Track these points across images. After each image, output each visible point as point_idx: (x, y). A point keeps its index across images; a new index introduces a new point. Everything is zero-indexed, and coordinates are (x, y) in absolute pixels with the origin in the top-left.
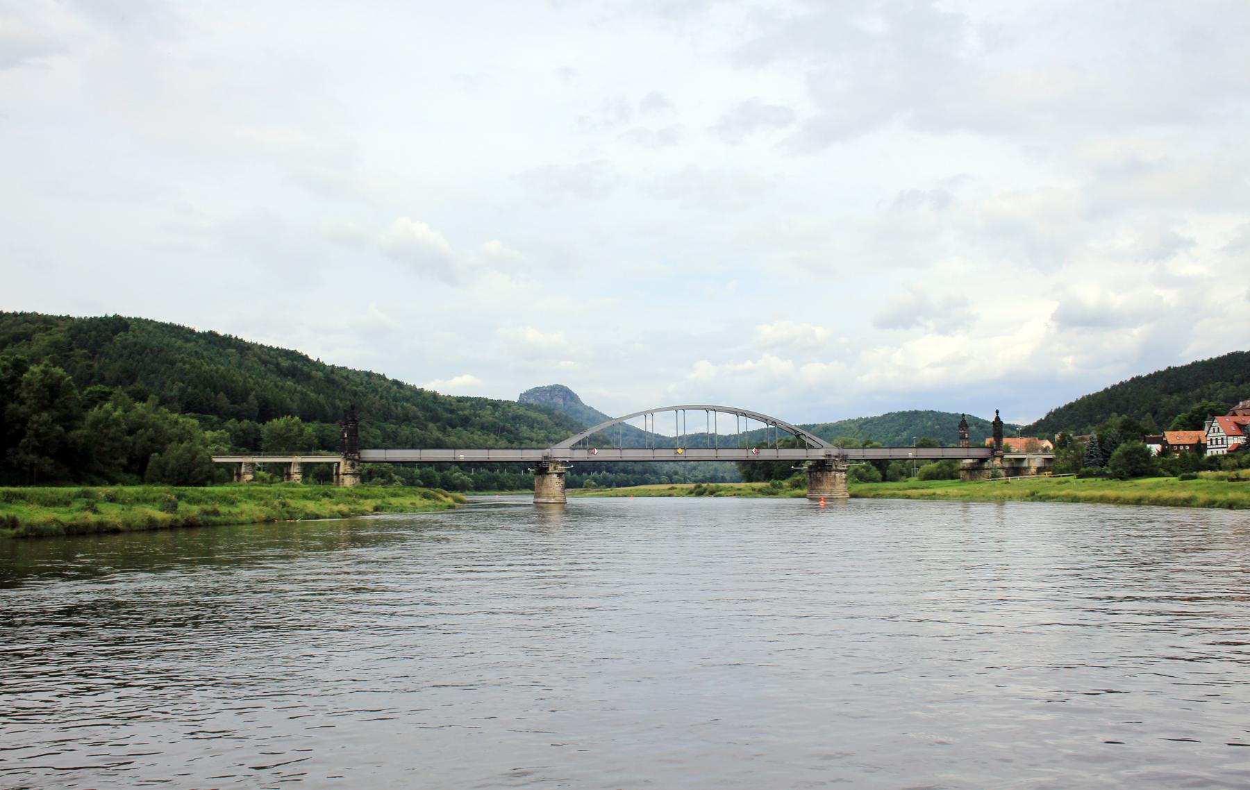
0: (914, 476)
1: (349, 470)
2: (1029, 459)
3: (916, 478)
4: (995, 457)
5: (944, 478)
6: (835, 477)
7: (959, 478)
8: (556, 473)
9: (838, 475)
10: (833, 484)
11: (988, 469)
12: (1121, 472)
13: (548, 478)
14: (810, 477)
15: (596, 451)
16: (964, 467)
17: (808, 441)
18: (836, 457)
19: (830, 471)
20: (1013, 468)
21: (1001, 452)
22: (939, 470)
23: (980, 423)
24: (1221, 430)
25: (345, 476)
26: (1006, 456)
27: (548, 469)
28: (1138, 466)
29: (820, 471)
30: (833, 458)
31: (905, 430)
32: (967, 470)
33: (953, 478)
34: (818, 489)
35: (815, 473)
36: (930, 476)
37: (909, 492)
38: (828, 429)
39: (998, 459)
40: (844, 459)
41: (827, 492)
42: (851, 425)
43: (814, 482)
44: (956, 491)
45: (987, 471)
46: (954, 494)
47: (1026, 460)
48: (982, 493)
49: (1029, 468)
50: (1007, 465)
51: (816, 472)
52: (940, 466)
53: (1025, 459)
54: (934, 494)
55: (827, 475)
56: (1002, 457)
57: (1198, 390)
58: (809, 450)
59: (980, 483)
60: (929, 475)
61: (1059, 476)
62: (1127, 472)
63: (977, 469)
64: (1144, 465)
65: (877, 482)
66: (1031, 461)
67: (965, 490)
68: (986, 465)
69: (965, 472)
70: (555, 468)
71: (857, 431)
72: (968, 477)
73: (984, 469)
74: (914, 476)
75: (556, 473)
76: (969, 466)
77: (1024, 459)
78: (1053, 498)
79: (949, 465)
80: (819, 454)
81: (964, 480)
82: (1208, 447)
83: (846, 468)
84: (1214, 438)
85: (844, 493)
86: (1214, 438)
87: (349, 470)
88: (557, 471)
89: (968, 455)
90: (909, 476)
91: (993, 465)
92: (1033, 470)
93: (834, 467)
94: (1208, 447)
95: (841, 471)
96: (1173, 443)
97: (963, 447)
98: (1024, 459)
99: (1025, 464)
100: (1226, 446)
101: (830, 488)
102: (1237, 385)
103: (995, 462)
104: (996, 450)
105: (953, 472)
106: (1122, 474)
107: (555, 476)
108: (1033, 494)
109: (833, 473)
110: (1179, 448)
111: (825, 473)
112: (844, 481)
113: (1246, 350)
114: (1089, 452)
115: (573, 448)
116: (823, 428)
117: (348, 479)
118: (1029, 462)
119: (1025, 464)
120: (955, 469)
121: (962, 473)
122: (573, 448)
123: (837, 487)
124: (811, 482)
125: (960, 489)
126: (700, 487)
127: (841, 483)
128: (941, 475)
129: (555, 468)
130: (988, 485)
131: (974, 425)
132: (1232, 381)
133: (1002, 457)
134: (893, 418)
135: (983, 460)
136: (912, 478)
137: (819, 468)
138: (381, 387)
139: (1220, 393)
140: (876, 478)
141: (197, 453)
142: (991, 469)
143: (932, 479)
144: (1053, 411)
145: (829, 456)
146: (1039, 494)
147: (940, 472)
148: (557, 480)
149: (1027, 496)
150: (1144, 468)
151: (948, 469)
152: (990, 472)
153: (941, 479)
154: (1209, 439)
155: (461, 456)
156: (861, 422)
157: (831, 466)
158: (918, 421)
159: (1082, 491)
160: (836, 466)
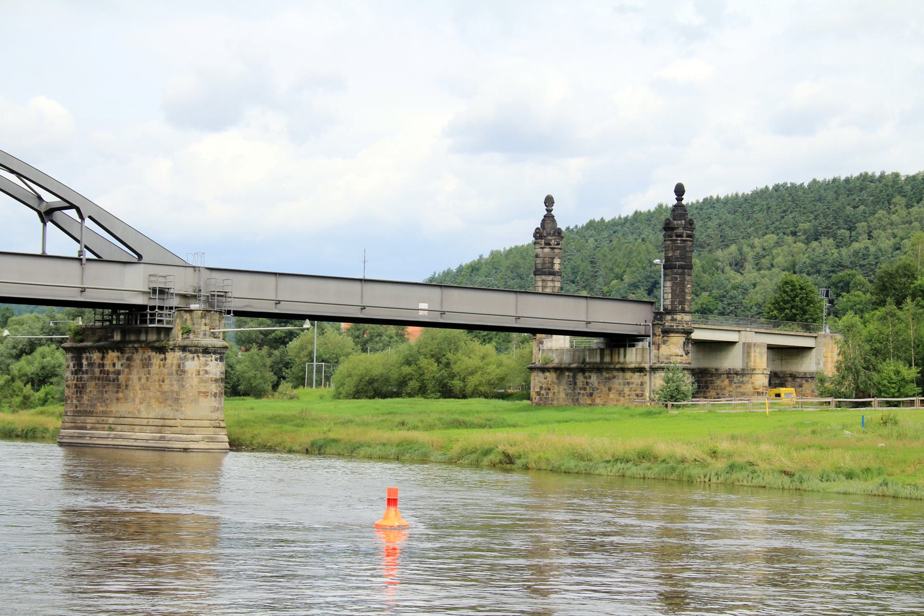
4: (666, 332)
6: (181, 371)
9: (193, 364)
14: (78, 369)
21: (687, 318)
22: (407, 370)
29: (119, 347)
30: (175, 302)
32: (559, 370)
34: (105, 414)
35: (96, 356)
39: (678, 340)
43: (91, 387)
47: (737, 351)
51: (103, 350)
53: (733, 343)
55: (146, 364)
57: (733, 248)
60: (371, 382)
63: (598, 369)
68: (632, 356)
69: (551, 376)
72: (561, 391)
73: (623, 370)
77: (729, 345)
81: (544, 402)
93: (177, 333)
95: (206, 351)
101: (157, 410)
102: (807, 242)
109: (173, 357)
111: (137, 357)
113: (907, 168)
123: (189, 410)
124: (80, 389)
127: (206, 394)
128: (413, 384)
132: (794, 234)
136: (307, 389)
137: (117, 337)
138: (106, 391)
139: (778, 254)
141: (252, 384)
151: (434, 367)
157: (168, 330)
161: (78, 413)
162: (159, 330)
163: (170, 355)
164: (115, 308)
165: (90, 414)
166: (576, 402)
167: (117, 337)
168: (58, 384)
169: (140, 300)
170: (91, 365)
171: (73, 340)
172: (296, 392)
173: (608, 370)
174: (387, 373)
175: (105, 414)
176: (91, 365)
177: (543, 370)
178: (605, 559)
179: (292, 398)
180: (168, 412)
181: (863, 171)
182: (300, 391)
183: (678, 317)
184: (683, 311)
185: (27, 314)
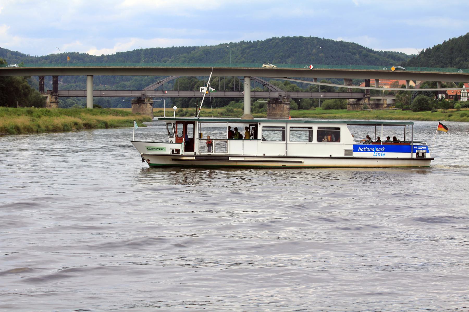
0: (319, 107)
1: (54, 101)
2: (383, 99)
3: (321, 108)
4: (366, 98)
5: (337, 108)
6: (284, 107)
7: (346, 109)
8: (149, 103)
9: (285, 106)
10: (283, 111)
11: (362, 104)
12: (416, 108)
13: (144, 106)
14: (269, 107)
15: (167, 92)
16: (349, 103)
17: (270, 88)
18: (284, 96)
19: (281, 104)
20: (375, 104)
21: (369, 95)
22: (334, 103)
23: (364, 52)
24: (466, 90)
25: (51, 104)
26: (371, 98)
27: (144, 101)
28: (423, 106)
29: (275, 103)
31: (289, 56)
32: (351, 104)
33: (342, 108)
35: (272, 105)
36: (329, 107)
37: (322, 115)
38: (209, 53)
40: (288, 98)
41: (279, 115)
42: (233, 49)
43: (271, 109)
44: (345, 115)
45: (361, 105)
46: (345, 116)
47: (382, 100)
48: (357, 116)
49: (383, 104)
50: (372, 102)
51: (273, 104)
52: (335, 102)
53: (381, 99)
54: (335, 116)
56: (369, 98)
58: (271, 93)
59: (357, 112)
61: (397, 109)
62: (418, 108)
63: (356, 104)
64: (426, 105)
65: (295, 109)
66: (384, 101)
67: (350, 115)
68: (361, 102)
69: (350, 105)
70: (149, 101)
71: (240, 56)
72: (351, 108)
73: (359, 104)
74: (320, 107)
75: (149, 103)
76: (352, 102)
78: (384, 118)
79: (340, 101)
80: (276, 95)
81: (349, 110)
82: (461, 97)
83: (289, 103)
84: (463, 93)
85: (288, 115)
86: (463, 93)
87: (54, 101)
88: (150, 102)
89: (352, 97)
90: (316, 106)
91: (364, 102)
92: (385, 105)
94: (461, 97)
95: (287, 104)
96: (450, 94)
97: (349, 92)
98: (381, 99)
99: (381, 102)
100: (467, 97)
101: (280, 112)
103: (366, 101)
104: (366, 95)
105: (342, 105)
106: (417, 109)
107: (149, 104)
108: (377, 117)
109: (282, 105)
110: (452, 97)
111: (278, 105)
112: (288, 109)
114: (413, 97)
115: (156, 90)
116: (204, 51)
117: (54, 105)
118: (383, 101)
119: (381, 102)
120: (343, 103)
121: (348, 106)
122: (156, 90)
123: (285, 112)
125: (347, 114)
126: (182, 111)
129: (149, 101)
130: (360, 113)
131: (357, 55)
133: (369, 98)
134: (277, 43)
135: (359, 100)
136: (318, 108)
137: (275, 102)
140: (294, 107)
142: (363, 104)
143: (330, 109)
144: (424, 51)
145: (281, 96)
146: (380, 117)
147: (335, 105)
148: (150, 107)
149: (375, 118)
150: (426, 107)
152: (363, 106)
153: (335, 109)
154: (461, 93)
155: (103, 94)
156: (244, 46)
157: (282, 101)
158: (303, 48)
159: (393, 115)
160: (284, 101)
161: (270, 113)
162: (280, 101)
163: (282, 105)
164: (274, 98)
165: (271, 113)
166: (353, 110)
167: (275, 102)
168: (264, 108)
169: (277, 97)
170: (271, 106)
171: (268, 102)
172: (315, 108)
173: (358, 104)
174: (140, 106)
175: (273, 113)
176: (271, 106)
177: (348, 104)
178: (29, 177)
179: (314, 110)
180: (282, 113)
181: (258, 40)
182: (316, 108)
183: (367, 95)
184: (368, 94)
185: (181, 98)
